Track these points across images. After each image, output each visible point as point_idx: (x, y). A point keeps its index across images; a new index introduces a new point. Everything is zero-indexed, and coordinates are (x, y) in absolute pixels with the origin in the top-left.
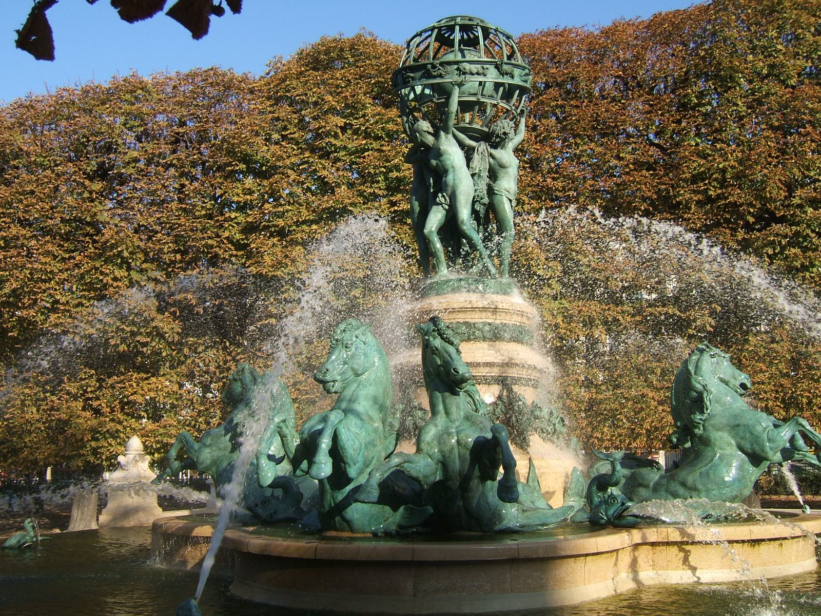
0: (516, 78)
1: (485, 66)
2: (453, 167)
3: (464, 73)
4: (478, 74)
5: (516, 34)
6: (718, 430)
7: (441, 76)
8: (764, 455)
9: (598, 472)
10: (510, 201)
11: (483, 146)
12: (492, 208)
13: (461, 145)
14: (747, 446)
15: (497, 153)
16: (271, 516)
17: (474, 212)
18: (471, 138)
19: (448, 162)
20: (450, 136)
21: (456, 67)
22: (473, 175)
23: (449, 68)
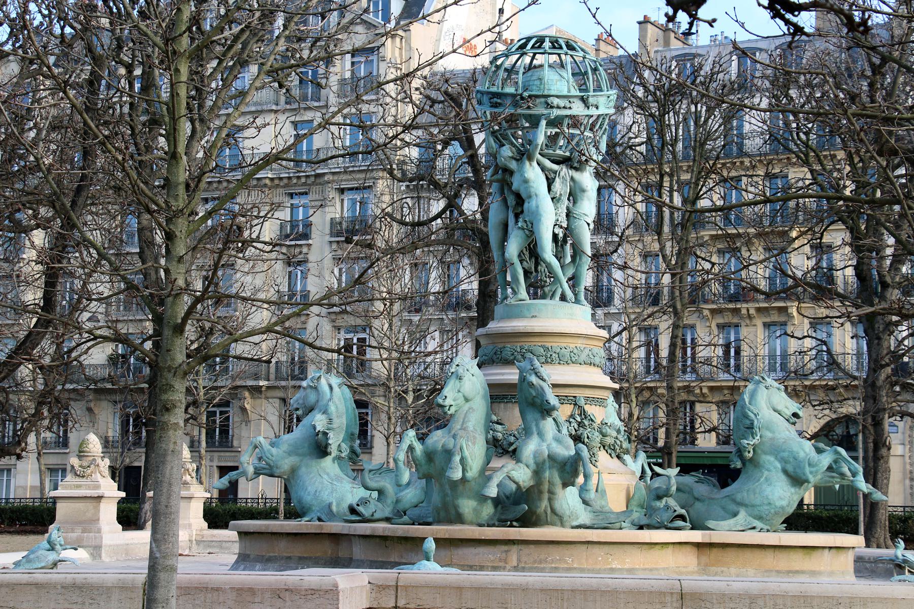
0: (600, 108)
1: (571, 100)
2: (536, 195)
3: (552, 107)
4: (564, 107)
5: (597, 184)
6: (766, 453)
7: (529, 108)
8: (804, 477)
9: (141, 559)
10: (588, 224)
11: (564, 170)
12: (569, 231)
13: (543, 169)
14: (790, 468)
15: (577, 175)
16: (373, 515)
17: (555, 236)
18: (553, 162)
19: (532, 190)
20: (535, 164)
21: (543, 100)
22: (552, 199)
23: (538, 100)
